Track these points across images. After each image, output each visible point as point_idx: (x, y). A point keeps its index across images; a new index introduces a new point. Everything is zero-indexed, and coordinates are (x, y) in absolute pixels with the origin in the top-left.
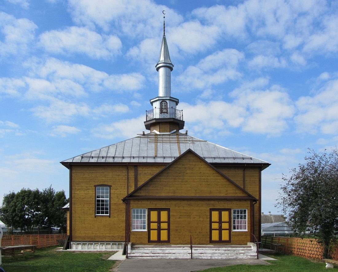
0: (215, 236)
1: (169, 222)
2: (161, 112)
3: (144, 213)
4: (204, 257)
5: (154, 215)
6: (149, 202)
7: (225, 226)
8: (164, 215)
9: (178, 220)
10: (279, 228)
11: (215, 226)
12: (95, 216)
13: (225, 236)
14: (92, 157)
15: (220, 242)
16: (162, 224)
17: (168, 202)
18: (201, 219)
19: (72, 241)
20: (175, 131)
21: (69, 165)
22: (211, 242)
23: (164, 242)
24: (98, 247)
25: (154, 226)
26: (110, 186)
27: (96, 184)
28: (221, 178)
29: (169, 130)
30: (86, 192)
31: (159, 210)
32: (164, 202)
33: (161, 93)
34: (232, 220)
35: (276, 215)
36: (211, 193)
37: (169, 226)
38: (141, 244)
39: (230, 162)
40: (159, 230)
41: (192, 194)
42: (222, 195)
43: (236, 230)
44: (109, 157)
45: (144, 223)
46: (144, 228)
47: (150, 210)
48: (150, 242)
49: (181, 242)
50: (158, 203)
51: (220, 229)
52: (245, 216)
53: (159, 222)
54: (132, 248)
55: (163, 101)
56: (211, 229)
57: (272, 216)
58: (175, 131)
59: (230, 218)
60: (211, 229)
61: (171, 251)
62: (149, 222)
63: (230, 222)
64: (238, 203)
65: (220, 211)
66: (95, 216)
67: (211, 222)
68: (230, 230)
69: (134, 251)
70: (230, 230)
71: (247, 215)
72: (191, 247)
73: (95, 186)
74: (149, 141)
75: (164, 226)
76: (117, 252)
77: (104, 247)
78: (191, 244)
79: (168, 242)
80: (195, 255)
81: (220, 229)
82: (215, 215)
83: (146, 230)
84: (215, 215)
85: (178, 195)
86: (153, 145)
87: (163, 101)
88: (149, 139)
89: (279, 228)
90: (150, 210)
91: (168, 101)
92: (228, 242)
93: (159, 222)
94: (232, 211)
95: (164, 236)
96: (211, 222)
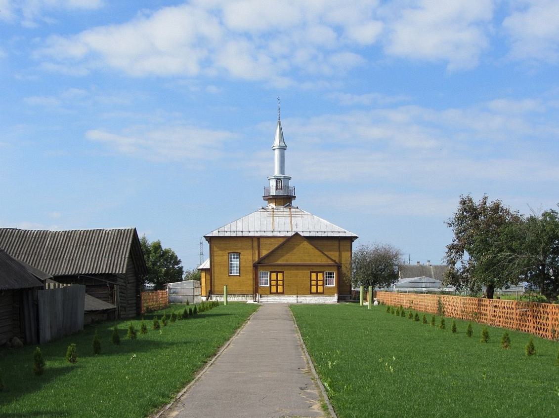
0: (314, 289)
1: (283, 280)
2: (277, 188)
3: (267, 274)
4: (304, 302)
5: (274, 275)
6: (270, 267)
7: (320, 283)
8: (280, 276)
9: (289, 279)
10: (416, 285)
11: (314, 283)
12: (229, 276)
13: (320, 289)
14: (226, 232)
15: (317, 293)
16: (279, 282)
17: (283, 267)
18: (305, 278)
19: (212, 294)
20: (288, 204)
21: (210, 239)
22: (311, 293)
23: (280, 293)
24: (232, 299)
25: (274, 283)
26: (240, 253)
27: (229, 251)
28: (317, 251)
29: (283, 204)
30: (222, 258)
31: (277, 273)
32: (280, 268)
33: (277, 173)
34: (325, 279)
35: (437, 266)
36: (311, 261)
37: (283, 283)
38: (266, 294)
39: (329, 235)
40: (277, 285)
41: (299, 262)
42: (319, 263)
43: (327, 286)
44: (239, 231)
45: (267, 281)
46: (267, 284)
47: (271, 272)
48: (271, 293)
49: (291, 293)
50: (278, 269)
51: (317, 285)
52: (333, 276)
53: (277, 280)
54: (261, 297)
55: (278, 180)
56: (311, 285)
57: (431, 267)
58: (288, 204)
59: (323, 278)
60: (311, 285)
61: (284, 299)
62: (271, 280)
63: (323, 280)
64: (329, 267)
65: (317, 273)
66: (229, 276)
67: (311, 280)
68: (323, 285)
69: (262, 299)
70: (323, 285)
71: (334, 276)
72: (297, 296)
73: (229, 253)
74: (267, 215)
75: (280, 283)
76: (72, 368)
77: (236, 298)
78: (297, 294)
79: (283, 293)
80: (299, 301)
81: (317, 285)
82: (314, 275)
83: (269, 286)
84: (274, 275)
85: (289, 263)
86: (271, 219)
87: (278, 180)
88: (267, 213)
89: (416, 285)
90: (271, 272)
91: (282, 180)
92: (323, 293)
93: (277, 280)
94: (325, 274)
95: (280, 290)
96: (311, 280)
